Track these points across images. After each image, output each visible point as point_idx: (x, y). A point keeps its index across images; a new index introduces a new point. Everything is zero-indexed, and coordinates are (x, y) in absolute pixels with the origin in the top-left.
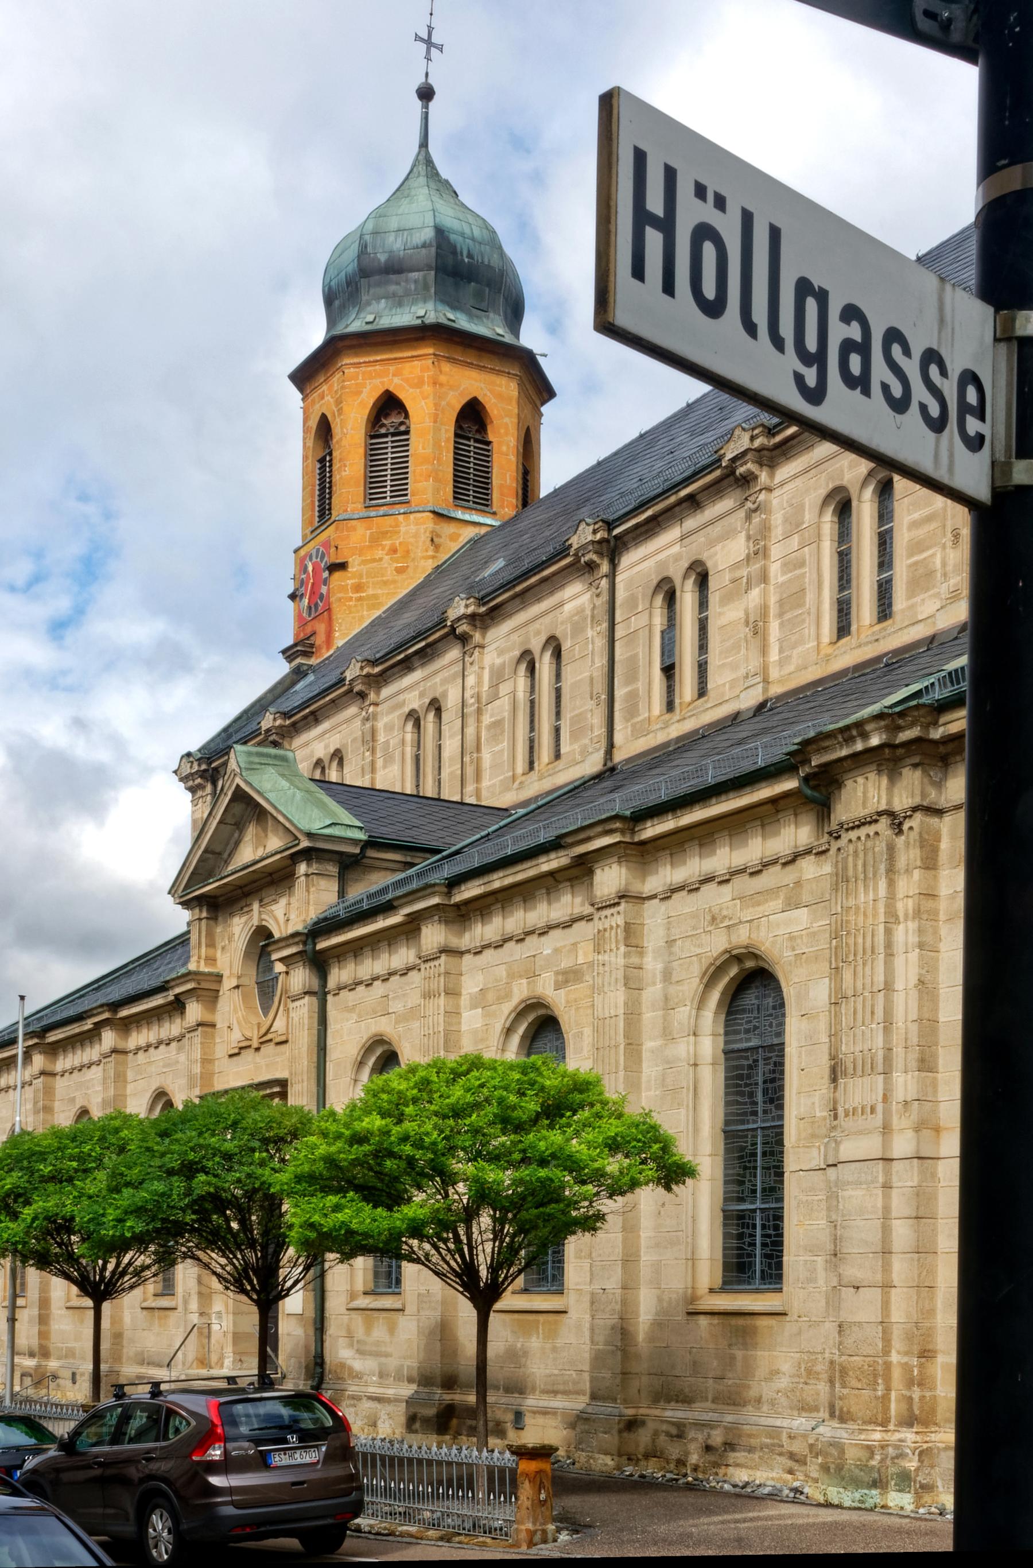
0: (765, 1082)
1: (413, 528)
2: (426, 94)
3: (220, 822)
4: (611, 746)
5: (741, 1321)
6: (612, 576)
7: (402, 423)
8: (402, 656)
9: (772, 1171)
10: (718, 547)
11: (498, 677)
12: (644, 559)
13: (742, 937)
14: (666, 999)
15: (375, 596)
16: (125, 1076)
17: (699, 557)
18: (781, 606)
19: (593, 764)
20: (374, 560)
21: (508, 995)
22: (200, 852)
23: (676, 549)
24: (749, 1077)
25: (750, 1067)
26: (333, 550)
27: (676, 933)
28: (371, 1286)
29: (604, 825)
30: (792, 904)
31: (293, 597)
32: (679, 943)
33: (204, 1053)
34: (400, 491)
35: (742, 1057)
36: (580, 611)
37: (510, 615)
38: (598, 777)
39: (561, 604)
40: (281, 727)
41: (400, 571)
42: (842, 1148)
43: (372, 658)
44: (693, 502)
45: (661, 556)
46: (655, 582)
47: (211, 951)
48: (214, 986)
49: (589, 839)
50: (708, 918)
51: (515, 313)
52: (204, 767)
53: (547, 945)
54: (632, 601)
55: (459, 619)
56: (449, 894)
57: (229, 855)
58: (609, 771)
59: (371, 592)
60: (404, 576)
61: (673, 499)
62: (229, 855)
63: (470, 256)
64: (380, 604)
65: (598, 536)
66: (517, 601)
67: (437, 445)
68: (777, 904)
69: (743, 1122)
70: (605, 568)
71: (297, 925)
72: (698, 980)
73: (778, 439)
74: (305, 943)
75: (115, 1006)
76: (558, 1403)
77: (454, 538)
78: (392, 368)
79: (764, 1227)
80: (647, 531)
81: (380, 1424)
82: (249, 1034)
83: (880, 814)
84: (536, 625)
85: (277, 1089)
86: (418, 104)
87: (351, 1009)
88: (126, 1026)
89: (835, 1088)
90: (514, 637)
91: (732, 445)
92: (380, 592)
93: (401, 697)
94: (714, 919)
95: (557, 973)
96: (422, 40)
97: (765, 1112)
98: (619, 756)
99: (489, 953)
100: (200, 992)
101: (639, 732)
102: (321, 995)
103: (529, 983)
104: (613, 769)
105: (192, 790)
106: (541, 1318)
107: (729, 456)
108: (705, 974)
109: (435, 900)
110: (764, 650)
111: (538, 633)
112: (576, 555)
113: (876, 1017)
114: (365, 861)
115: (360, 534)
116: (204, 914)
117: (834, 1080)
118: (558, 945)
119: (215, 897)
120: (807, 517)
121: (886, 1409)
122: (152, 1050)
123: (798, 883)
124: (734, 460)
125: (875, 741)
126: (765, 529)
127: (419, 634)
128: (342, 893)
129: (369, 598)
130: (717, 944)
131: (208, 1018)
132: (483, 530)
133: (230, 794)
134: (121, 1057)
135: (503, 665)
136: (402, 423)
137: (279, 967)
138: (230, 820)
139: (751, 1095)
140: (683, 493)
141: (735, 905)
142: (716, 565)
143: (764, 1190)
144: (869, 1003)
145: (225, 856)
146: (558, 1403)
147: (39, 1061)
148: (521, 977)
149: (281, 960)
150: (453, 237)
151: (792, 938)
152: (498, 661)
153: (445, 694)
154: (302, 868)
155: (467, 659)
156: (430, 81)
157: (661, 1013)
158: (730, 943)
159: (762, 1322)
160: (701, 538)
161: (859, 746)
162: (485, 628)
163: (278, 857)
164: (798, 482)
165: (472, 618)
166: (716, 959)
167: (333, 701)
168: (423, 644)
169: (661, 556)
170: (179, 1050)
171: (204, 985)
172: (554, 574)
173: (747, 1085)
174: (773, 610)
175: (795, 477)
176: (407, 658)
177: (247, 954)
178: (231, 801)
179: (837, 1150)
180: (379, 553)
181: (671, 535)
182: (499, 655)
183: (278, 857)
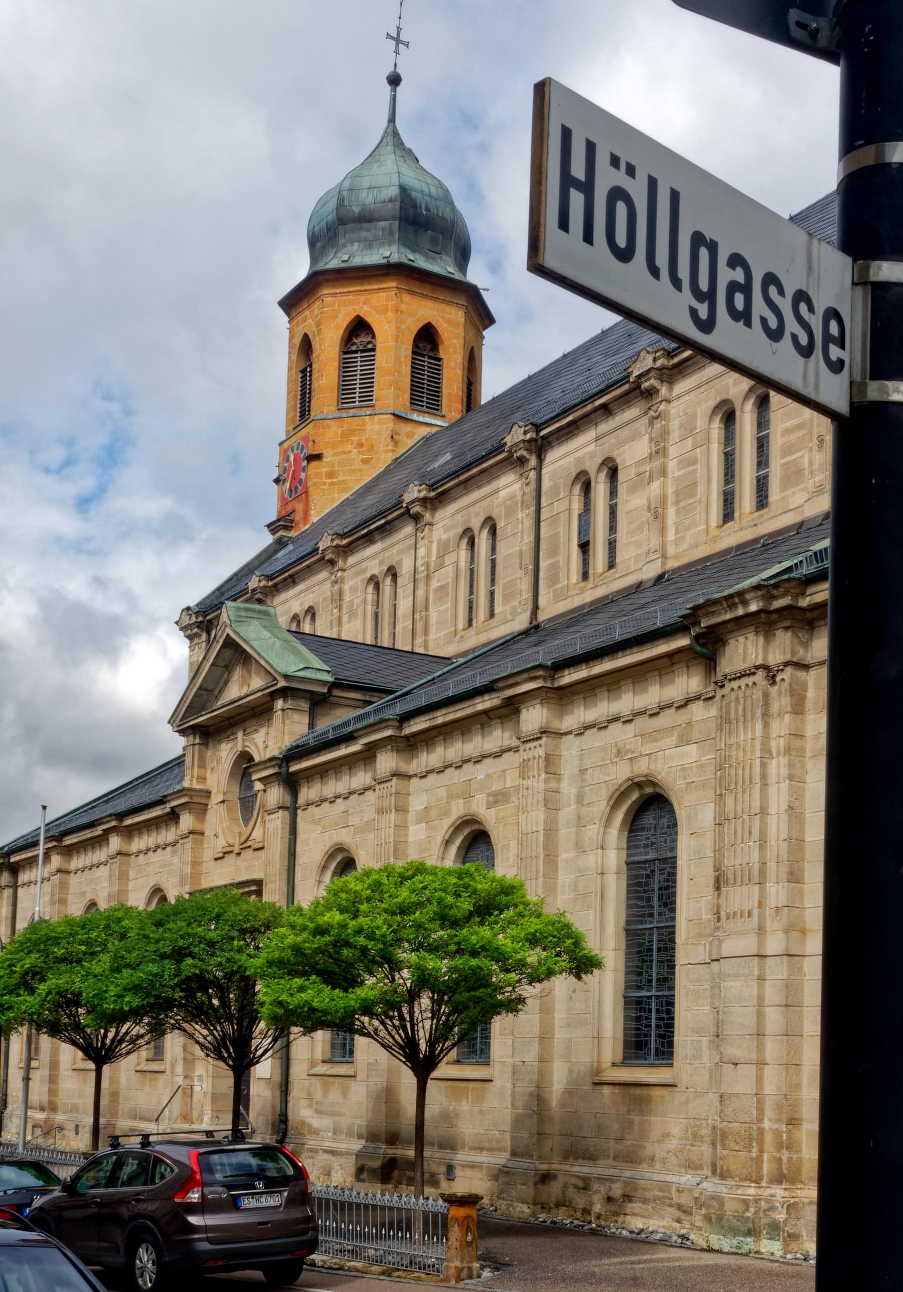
0: (660, 889)
1: (376, 427)
2: (394, 80)
3: (213, 665)
4: (536, 608)
5: (638, 1091)
6: (539, 469)
7: (369, 342)
8: (365, 531)
9: (665, 964)
10: (626, 447)
11: (444, 549)
12: (566, 455)
13: (642, 768)
14: (579, 818)
15: (344, 482)
16: (128, 874)
17: (611, 455)
18: (677, 496)
19: (521, 622)
20: (345, 453)
21: (447, 813)
22: (195, 689)
23: (592, 447)
24: (647, 884)
25: (648, 876)
26: (311, 443)
27: (587, 763)
28: (328, 1055)
29: (530, 672)
30: (684, 741)
31: (277, 481)
32: (590, 771)
33: (194, 857)
34: (367, 397)
35: (641, 868)
36: (512, 497)
37: (454, 500)
38: (525, 633)
39: (497, 491)
40: (265, 587)
41: (365, 461)
42: (724, 945)
43: (341, 532)
44: (606, 410)
45: (579, 454)
46: (574, 474)
47: (202, 772)
48: (203, 801)
49: (517, 684)
50: (615, 751)
51: (463, 255)
52: (200, 619)
53: (480, 772)
54: (555, 489)
55: (413, 502)
56: (400, 728)
57: (219, 692)
58: (534, 628)
59: (341, 478)
60: (369, 466)
61: (589, 407)
62: (219, 692)
63: (427, 209)
64: (349, 488)
65: (528, 436)
66: (461, 487)
67: (398, 360)
68: (671, 741)
69: (641, 923)
70: (533, 462)
71: (274, 751)
72: (605, 803)
73: (676, 360)
74: (280, 766)
75: (121, 816)
76: (484, 1158)
77: (410, 435)
78: (362, 298)
79: (658, 1011)
80: (568, 433)
81: (333, 1173)
82: (231, 841)
83: (757, 667)
84: (476, 508)
85: (254, 888)
86: (388, 88)
87: (317, 822)
88: (129, 832)
89: (719, 895)
90: (458, 517)
91: (638, 364)
92: (348, 478)
93: (364, 565)
94: (619, 752)
95: (489, 795)
96: (392, 38)
97: (660, 914)
98: (542, 617)
99: (432, 778)
100: (192, 806)
101: (559, 596)
102: (293, 810)
103: (465, 803)
104: (537, 627)
105: (190, 638)
106: (471, 1085)
107: (636, 373)
108: (611, 798)
109: (389, 733)
110: (663, 532)
111: (478, 514)
112: (510, 451)
113: (753, 836)
114: (331, 699)
115: (333, 431)
116: (197, 741)
117: (718, 888)
118: (490, 771)
119: (207, 727)
120: (699, 424)
121: (760, 1168)
122: (151, 853)
123: (689, 724)
124: (640, 377)
125: (753, 607)
126: (665, 433)
127: (380, 513)
128: (311, 725)
129: (339, 483)
130: (621, 773)
131: (198, 827)
132: (434, 430)
133: (221, 641)
134: (125, 858)
135: (449, 539)
136: (369, 342)
137: (258, 786)
138: (221, 663)
139: (649, 899)
140: (598, 403)
141: (637, 741)
142: (624, 461)
143: (658, 980)
144: (747, 825)
145: (216, 692)
146: (484, 1158)
147: (56, 860)
148: (458, 797)
149: (260, 780)
150: (414, 194)
151: (683, 769)
152: (444, 537)
153: (400, 563)
154: (279, 704)
155: (419, 534)
156: (398, 70)
157: (574, 829)
158: (632, 772)
159: (656, 1092)
160: (612, 439)
161: (740, 611)
162: (434, 509)
163: (260, 694)
164: (692, 395)
165: (424, 501)
166: (620, 786)
167: (308, 567)
168: (383, 521)
169: (579, 454)
170: (174, 853)
171: (195, 800)
172: (491, 466)
173: (645, 891)
174: (671, 499)
175: (689, 391)
176: (370, 533)
177: (232, 774)
178: (222, 647)
179: (719, 947)
180: (349, 447)
181: (588, 436)
182: (445, 532)
183: (260, 694)
